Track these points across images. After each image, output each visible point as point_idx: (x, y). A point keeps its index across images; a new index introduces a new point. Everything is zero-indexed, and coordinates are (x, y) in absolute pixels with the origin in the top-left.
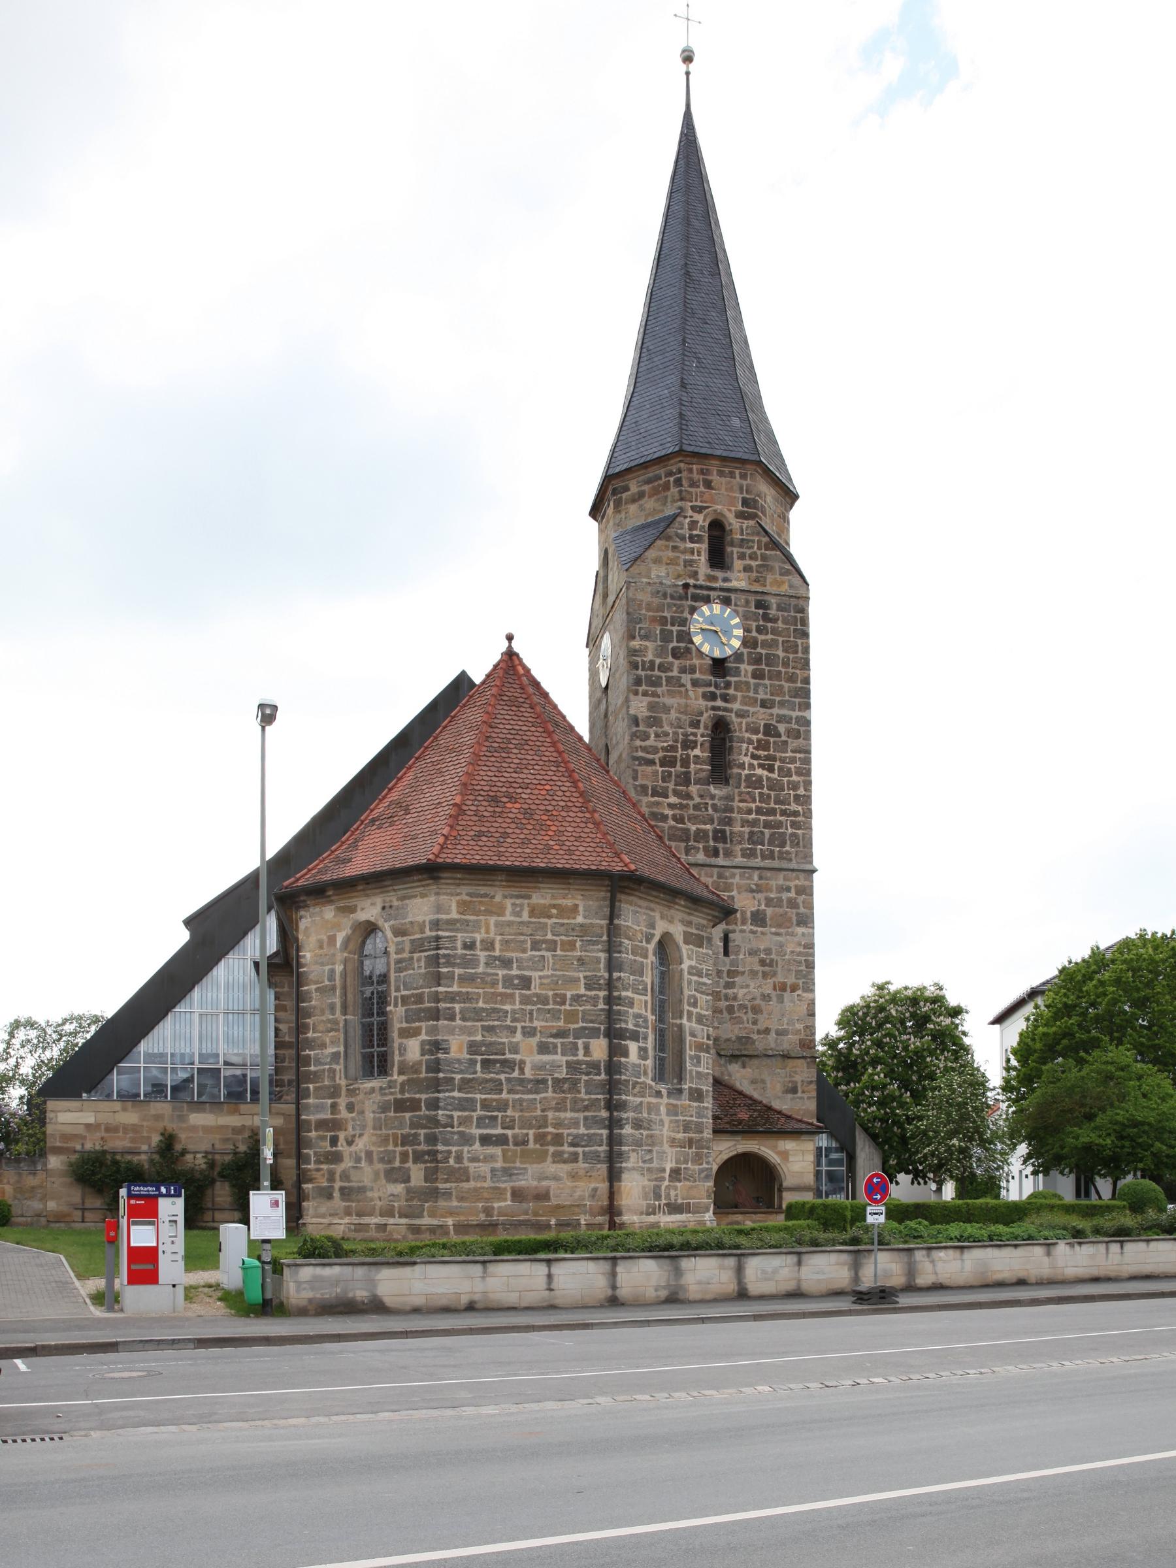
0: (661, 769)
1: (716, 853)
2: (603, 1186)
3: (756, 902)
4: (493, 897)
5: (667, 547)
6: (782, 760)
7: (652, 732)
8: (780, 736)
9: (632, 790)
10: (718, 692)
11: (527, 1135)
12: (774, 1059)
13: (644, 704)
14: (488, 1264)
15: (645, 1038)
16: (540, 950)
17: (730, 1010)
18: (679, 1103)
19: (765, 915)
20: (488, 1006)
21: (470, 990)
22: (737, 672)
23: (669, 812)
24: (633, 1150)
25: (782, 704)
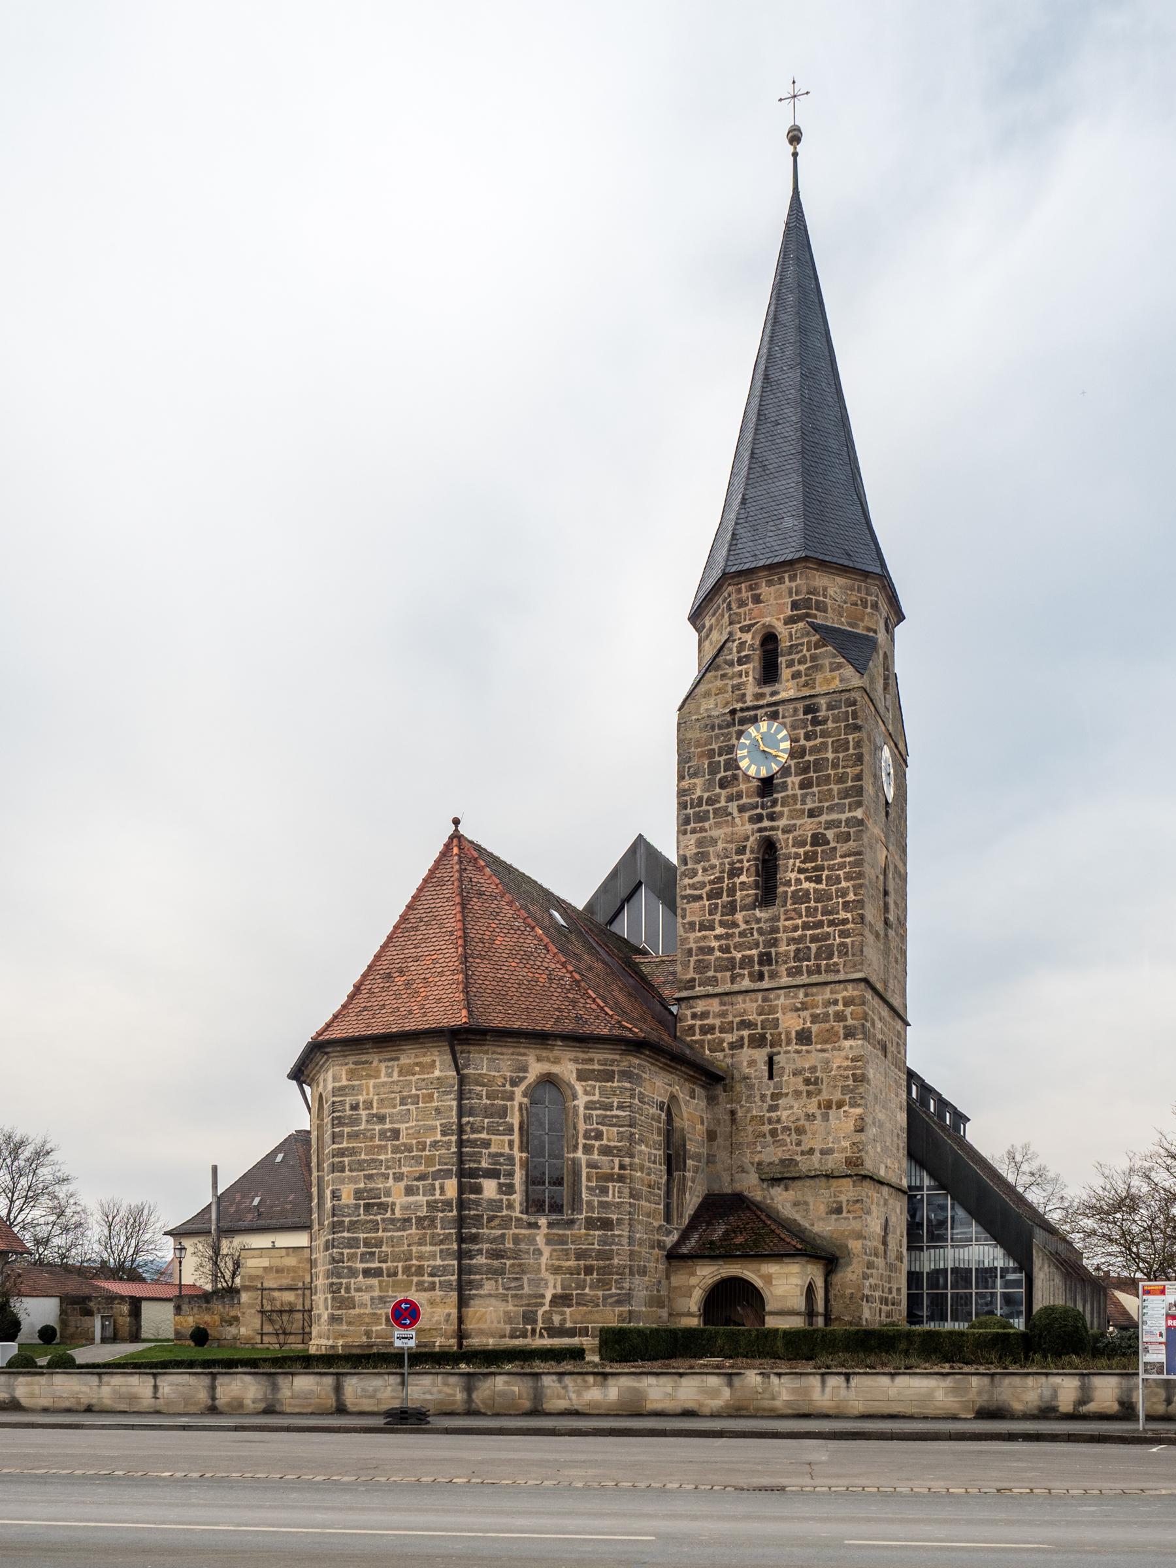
0: (708, 903)
1: (761, 977)
3: (802, 1021)
4: (371, 1063)
5: (716, 677)
6: (831, 868)
7: (699, 867)
9: (681, 928)
10: (764, 812)
11: (397, 1267)
12: (817, 1180)
13: (692, 842)
14: (826, 1376)
15: (511, 1174)
17: (773, 1132)
18: (568, 1232)
20: (368, 1158)
21: (355, 1145)
22: (784, 786)
24: (488, 1279)
25: (831, 809)
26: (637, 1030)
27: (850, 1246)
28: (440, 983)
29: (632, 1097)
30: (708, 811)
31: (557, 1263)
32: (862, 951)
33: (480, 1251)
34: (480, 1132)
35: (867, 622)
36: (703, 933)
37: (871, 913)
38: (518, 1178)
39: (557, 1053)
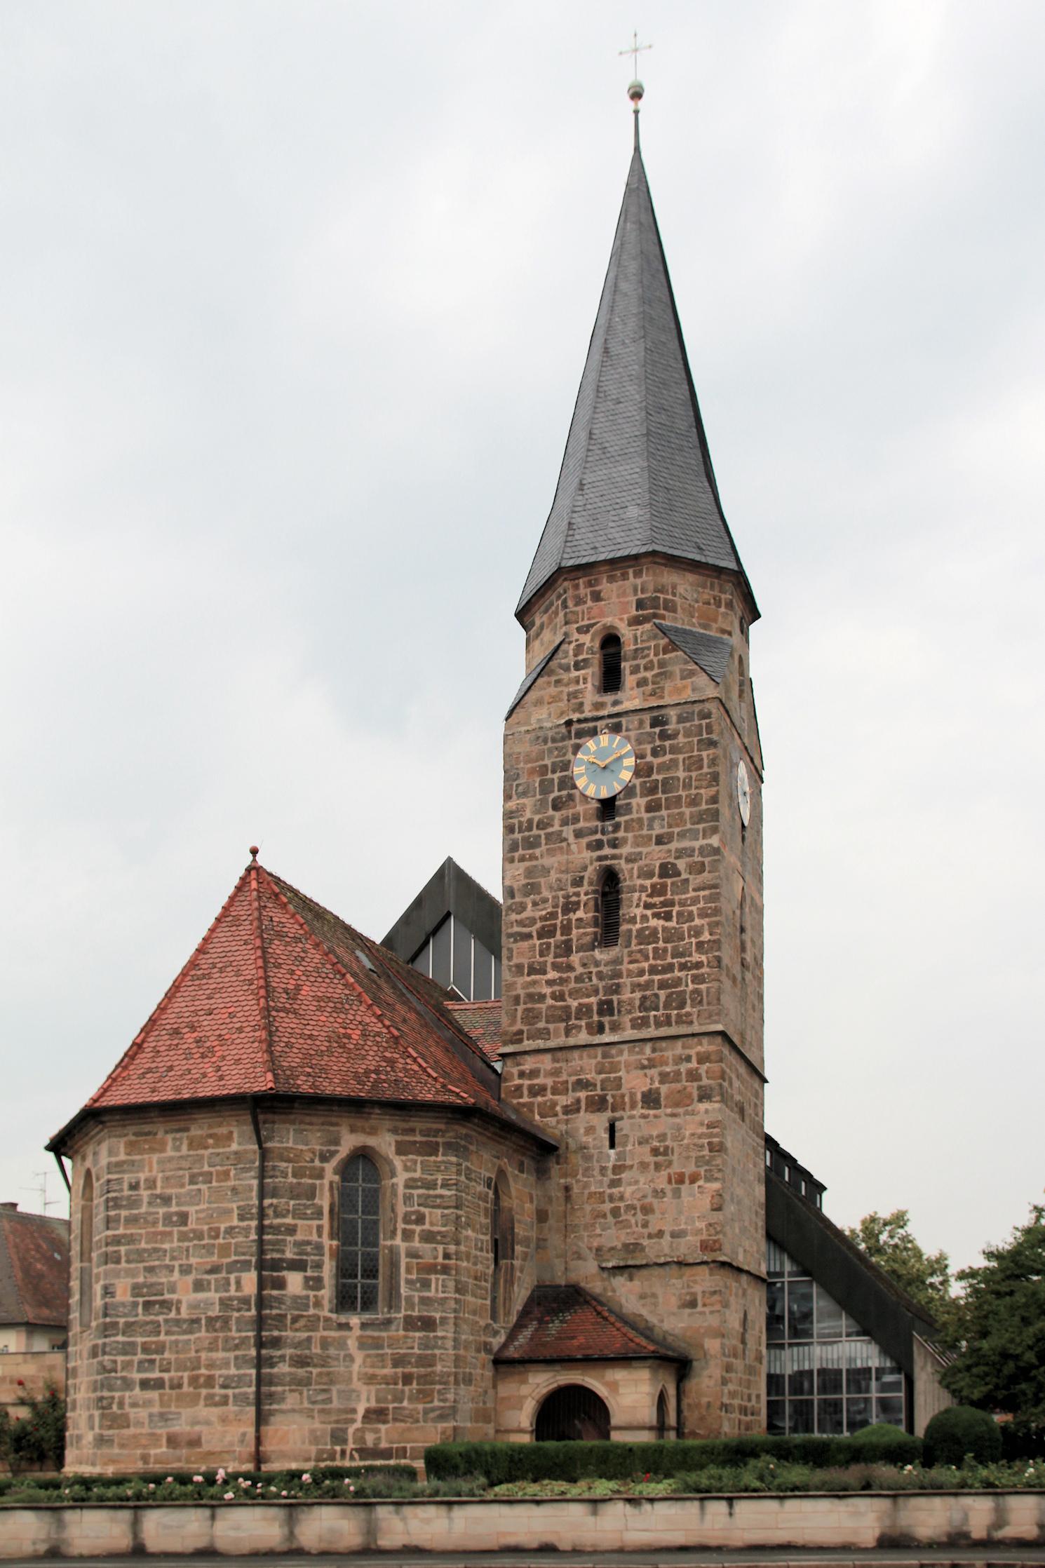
0: (538, 943)
1: (601, 1029)
2: (251, 1430)
3: (648, 1081)
4: (156, 1134)
5: (549, 683)
6: (682, 904)
7: (529, 901)
8: (678, 874)
9: (507, 972)
10: (605, 838)
11: (182, 1377)
12: (667, 1268)
13: (521, 871)
15: (318, 1266)
16: (197, 1183)
18: (384, 1334)
19: (659, 1094)
20: (149, 1246)
21: (133, 1231)
22: (628, 809)
23: (547, 990)
24: (291, 1391)
25: (682, 835)
26: (465, 1095)
27: (706, 1346)
28: (238, 1041)
29: (459, 1173)
30: (540, 836)
31: (371, 1371)
32: (719, 999)
33: (282, 1358)
34: (284, 1216)
35: (721, 623)
36: (533, 977)
37: (728, 954)
38: (328, 1270)
39: (373, 1122)
